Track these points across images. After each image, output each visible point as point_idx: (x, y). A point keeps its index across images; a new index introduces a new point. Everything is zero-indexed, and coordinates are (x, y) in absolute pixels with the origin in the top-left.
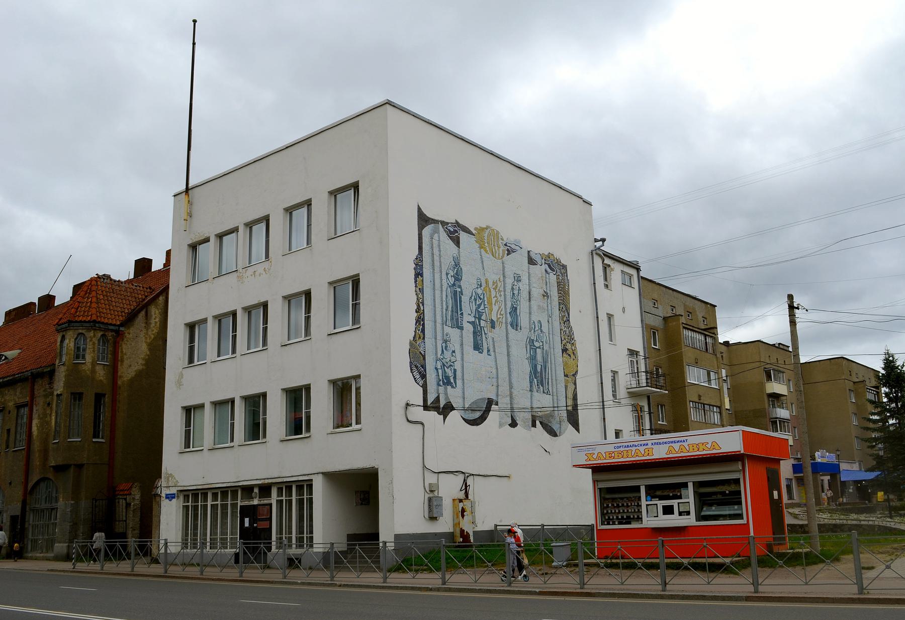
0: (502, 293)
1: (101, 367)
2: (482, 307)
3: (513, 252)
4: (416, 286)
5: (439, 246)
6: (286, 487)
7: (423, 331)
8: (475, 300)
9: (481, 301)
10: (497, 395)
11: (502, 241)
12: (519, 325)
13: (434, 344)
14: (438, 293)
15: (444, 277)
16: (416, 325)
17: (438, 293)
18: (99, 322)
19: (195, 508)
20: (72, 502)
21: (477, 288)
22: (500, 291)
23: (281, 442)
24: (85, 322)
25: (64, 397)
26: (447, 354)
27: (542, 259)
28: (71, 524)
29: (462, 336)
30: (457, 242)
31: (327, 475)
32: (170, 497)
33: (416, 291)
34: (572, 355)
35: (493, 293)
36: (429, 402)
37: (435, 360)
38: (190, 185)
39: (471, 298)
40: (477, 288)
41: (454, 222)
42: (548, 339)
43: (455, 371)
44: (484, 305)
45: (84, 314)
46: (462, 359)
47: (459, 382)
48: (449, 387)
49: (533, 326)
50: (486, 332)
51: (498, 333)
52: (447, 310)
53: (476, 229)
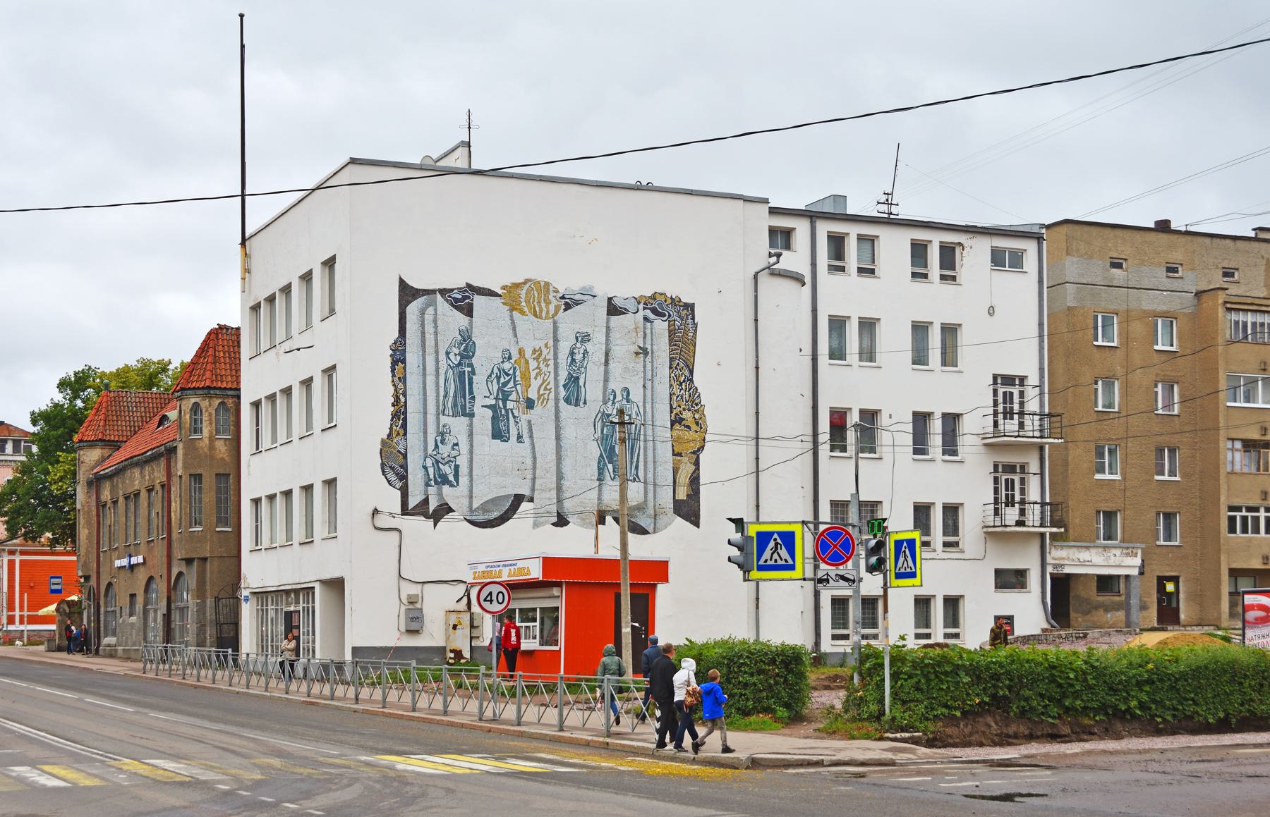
0: (551, 363)
1: (222, 442)
2: (511, 384)
3: (577, 304)
4: (393, 376)
5: (435, 321)
7: (404, 426)
8: (498, 378)
9: (507, 378)
10: (533, 490)
11: (555, 294)
12: (583, 398)
13: (422, 439)
14: (430, 380)
15: (442, 357)
16: (392, 420)
17: (430, 380)
18: (215, 388)
19: (262, 610)
20: (199, 601)
21: (503, 362)
22: (545, 360)
24: (198, 388)
25: (184, 479)
26: (445, 450)
27: (639, 303)
28: (199, 625)
29: (471, 425)
30: (468, 311)
31: (323, 582)
32: (247, 600)
33: (393, 381)
34: (694, 427)
35: (533, 364)
36: (411, 506)
37: (423, 458)
38: (247, 235)
39: (490, 376)
40: (503, 362)
41: (465, 285)
42: (641, 410)
43: (457, 467)
44: (515, 381)
45: (198, 378)
46: (471, 452)
47: (464, 480)
48: (446, 488)
49: (612, 397)
50: (516, 414)
51: (542, 415)
52: (445, 396)
53: (504, 288)
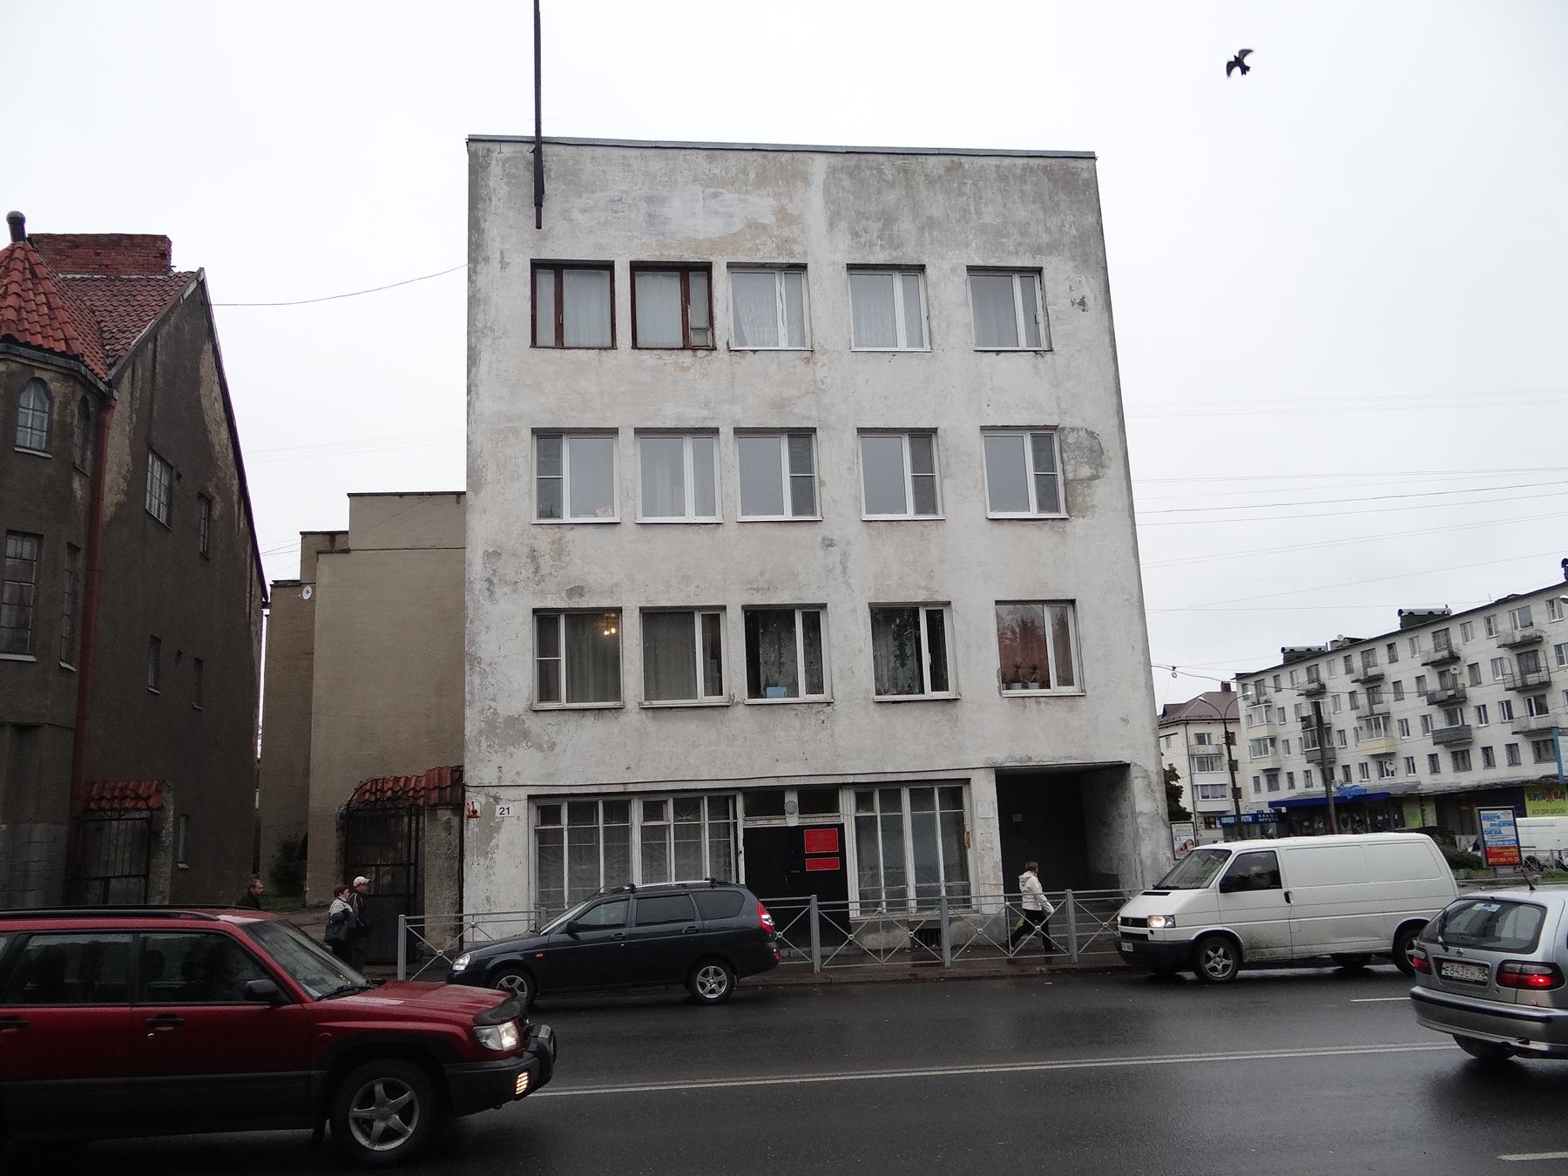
6: (921, 791)
23: (877, 707)
